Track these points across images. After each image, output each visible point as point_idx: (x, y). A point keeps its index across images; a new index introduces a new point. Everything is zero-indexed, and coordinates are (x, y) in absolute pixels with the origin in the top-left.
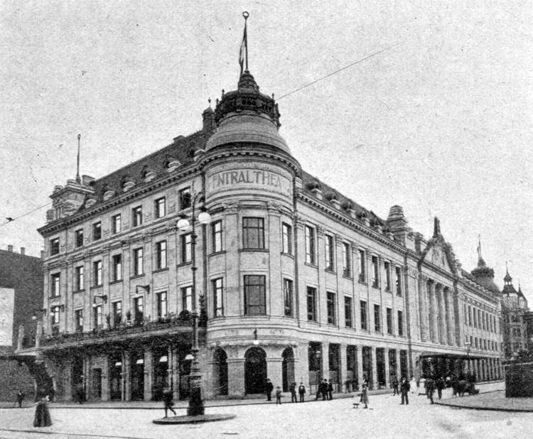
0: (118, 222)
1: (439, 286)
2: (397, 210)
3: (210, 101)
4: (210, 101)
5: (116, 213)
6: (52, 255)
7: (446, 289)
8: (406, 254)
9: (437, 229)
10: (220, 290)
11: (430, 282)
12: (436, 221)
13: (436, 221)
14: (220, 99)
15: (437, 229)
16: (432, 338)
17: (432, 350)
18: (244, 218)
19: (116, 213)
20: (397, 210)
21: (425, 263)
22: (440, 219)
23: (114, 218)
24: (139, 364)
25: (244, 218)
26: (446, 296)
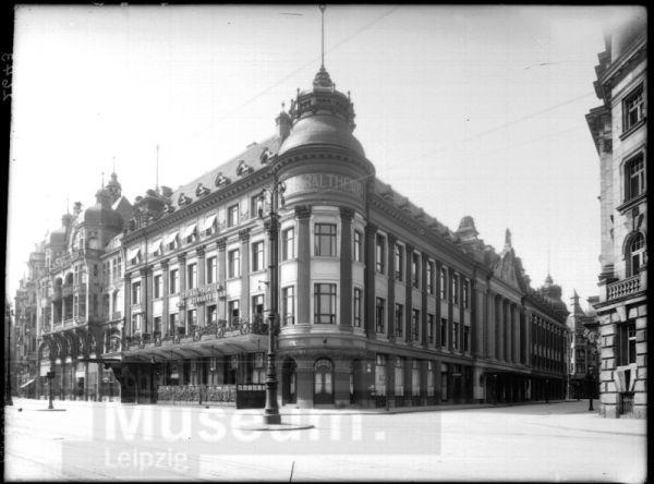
0: (235, 214)
1: (506, 301)
2: (468, 221)
3: (283, 105)
4: (283, 105)
5: (234, 203)
6: (533, 326)
7: (514, 305)
8: (476, 267)
9: (508, 240)
10: (322, 312)
11: (498, 297)
12: (508, 234)
13: (508, 234)
14: (295, 99)
15: (508, 240)
16: (505, 359)
17: (505, 368)
18: (316, 224)
19: (234, 203)
20: (468, 221)
21: (495, 278)
22: (511, 231)
23: (230, 209)
24: (174, 379)
25: (316, 224)
26: (512, 311)
